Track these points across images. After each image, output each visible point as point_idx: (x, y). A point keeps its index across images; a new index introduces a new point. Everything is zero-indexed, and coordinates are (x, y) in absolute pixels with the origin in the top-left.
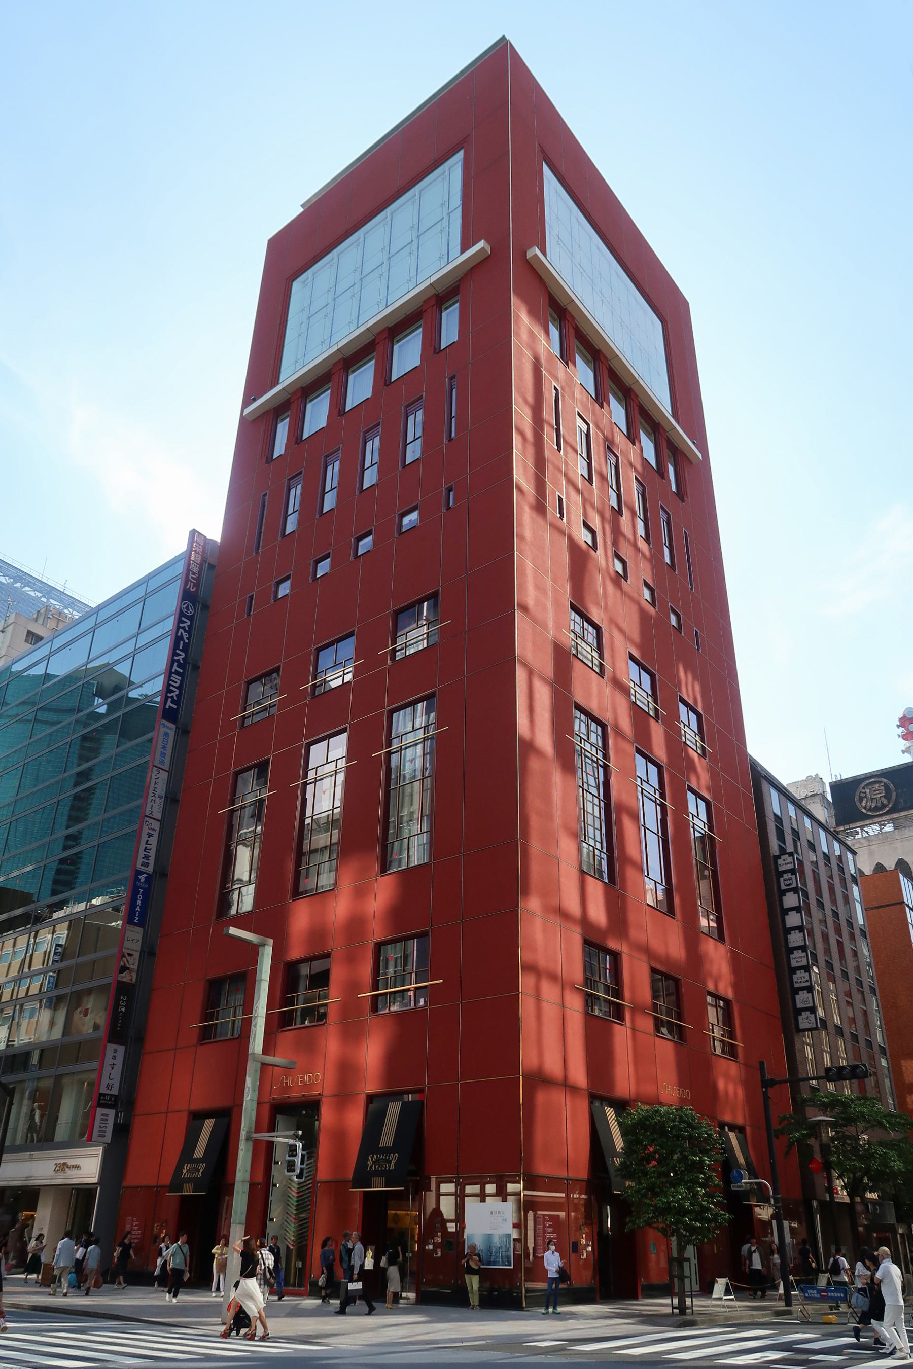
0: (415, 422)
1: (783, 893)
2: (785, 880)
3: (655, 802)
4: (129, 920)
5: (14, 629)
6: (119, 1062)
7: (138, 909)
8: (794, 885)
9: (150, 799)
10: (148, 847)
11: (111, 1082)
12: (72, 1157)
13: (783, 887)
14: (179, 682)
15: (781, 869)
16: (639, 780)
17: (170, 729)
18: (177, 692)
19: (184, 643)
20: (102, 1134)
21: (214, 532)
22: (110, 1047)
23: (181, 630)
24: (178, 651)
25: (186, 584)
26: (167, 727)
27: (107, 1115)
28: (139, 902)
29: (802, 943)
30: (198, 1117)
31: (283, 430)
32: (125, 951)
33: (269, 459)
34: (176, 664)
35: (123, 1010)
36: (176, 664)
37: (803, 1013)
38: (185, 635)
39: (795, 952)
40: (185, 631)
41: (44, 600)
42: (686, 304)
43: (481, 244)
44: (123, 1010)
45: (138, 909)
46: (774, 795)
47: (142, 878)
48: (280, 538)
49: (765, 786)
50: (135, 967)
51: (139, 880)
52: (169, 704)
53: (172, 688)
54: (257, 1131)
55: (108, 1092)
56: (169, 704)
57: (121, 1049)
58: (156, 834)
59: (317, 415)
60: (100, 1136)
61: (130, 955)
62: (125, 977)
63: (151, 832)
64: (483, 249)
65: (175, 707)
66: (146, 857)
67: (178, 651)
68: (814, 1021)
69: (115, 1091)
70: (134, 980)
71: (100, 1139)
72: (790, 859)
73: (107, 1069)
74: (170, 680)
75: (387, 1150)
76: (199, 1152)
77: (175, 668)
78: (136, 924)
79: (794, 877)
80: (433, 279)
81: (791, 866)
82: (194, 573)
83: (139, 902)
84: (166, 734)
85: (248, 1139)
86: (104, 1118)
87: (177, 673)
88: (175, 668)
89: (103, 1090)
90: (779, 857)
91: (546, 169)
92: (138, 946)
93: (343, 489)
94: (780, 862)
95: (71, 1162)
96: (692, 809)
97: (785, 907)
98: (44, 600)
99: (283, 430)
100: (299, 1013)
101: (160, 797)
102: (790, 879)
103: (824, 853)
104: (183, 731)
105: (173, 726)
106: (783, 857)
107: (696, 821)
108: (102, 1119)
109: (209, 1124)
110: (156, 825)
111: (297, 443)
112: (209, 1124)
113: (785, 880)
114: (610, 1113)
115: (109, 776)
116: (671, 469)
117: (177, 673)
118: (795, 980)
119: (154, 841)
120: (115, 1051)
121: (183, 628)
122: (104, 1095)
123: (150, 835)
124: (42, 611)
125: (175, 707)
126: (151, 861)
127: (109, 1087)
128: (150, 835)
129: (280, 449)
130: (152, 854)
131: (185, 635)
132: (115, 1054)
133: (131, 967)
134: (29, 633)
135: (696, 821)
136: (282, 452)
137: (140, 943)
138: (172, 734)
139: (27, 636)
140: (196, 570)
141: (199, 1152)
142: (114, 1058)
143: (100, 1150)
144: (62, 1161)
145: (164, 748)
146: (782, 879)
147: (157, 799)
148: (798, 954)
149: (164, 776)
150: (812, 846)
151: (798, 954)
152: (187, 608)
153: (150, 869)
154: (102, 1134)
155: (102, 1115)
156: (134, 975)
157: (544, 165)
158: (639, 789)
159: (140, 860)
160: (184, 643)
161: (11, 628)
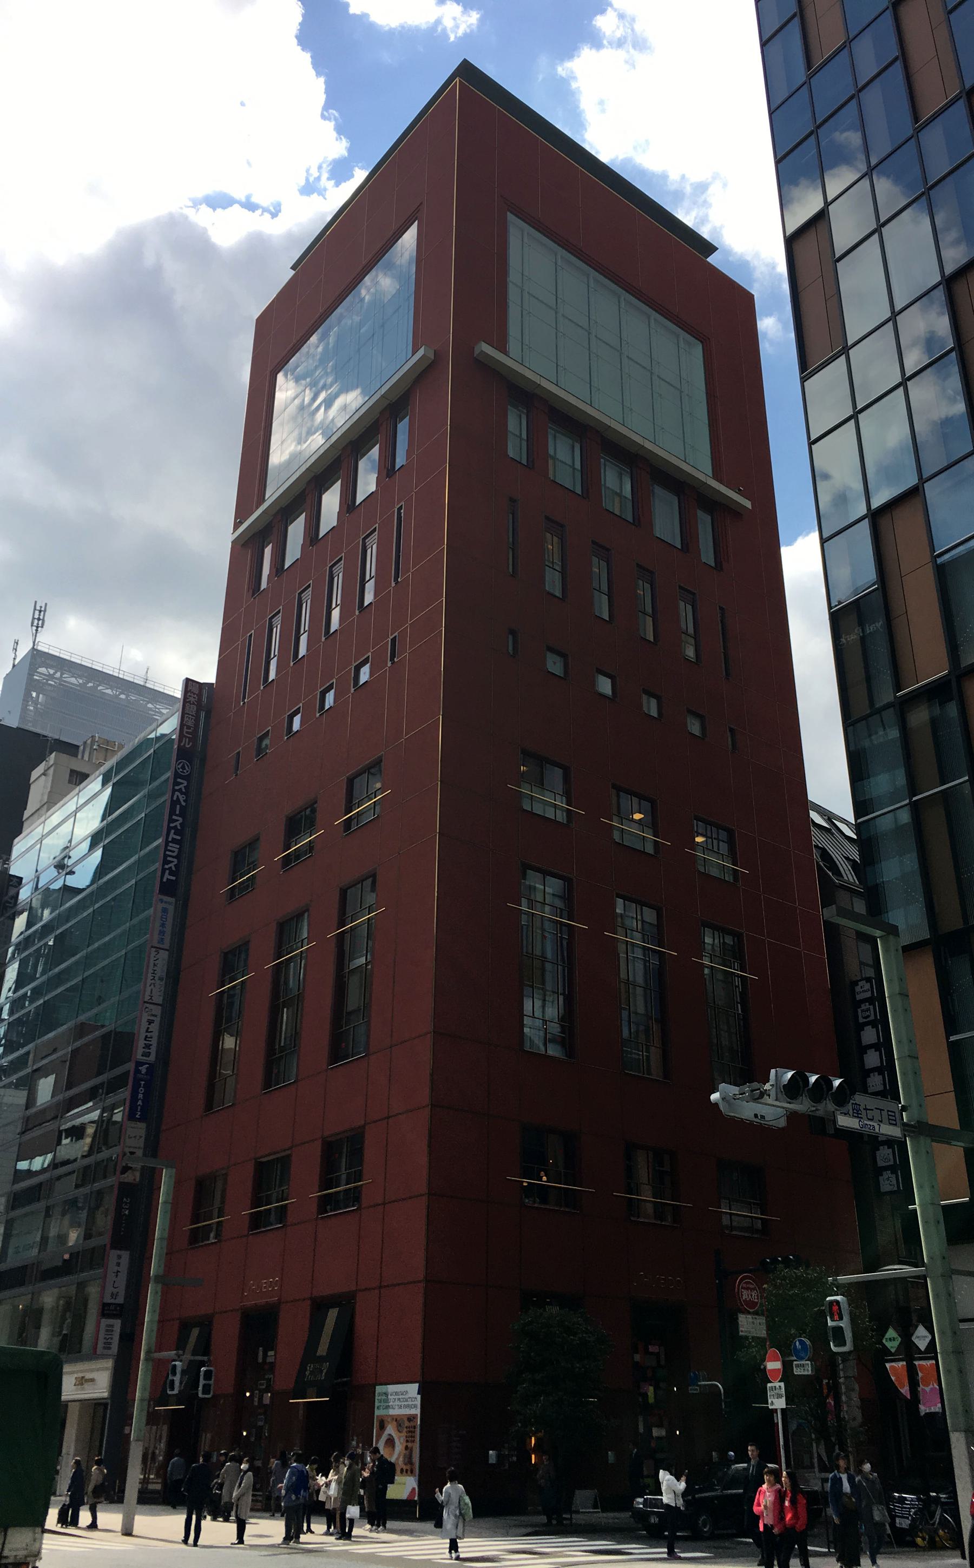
1: (861, 1027)
2: (862, 1011)
4: (131, 1116)
5: (55, 771)
6: (124, 1268)
7: (140, 1103)
8: (872, 1017)
9: (149, 982)
11: (115, 1291)
12: (92, 1371)
13: (861, 1020)
14: (176, 850)
17: (170, 903)
19: (181, 806)
20: (107, 1346)
22: (114, 1254)
24: (174, 817)
27: (112, 1326)
28: (141, 1096)
30: (319, 1306)
32: (127, 1150)
34: (173, 831)
35: (127, 1212)
36: (173, 831)
37: (884, 1173)
38: (182, 798)
40: (182, 793)
41: (123, 696)
44: (127, 1212)
45: (140, 1103)
47: (143, 1069)
48: (357, 612)
51: (140, 1072)
53: (169, 859)
54: (159, 1348)
55: (113, 1301)
56: (167, 876)
57: (125, 1255)
58: (157, 1020)
60: (104, 1348)
61: (132, 1153)
62: (129, 1177)
63: (152, 1018)
65: (174, 878)
67: (174, 817)
68: (895, 1182)
69: (120, 1300)
70: (138, 1180)
71: (106, 1352)
73: (111, 1277)
75: (321, 1359)
76: (322, 1350)
77: (172, 835)
78: (140, 1120)
79: (871, 1007)
81: (869, 994)
82: (189, 727)
83: (141, 1096)
85: (146, 1359)
86: (110, 1329)
87: (174, 841)
88: (172, 835)
89: (108, 1300)
92: (141, 1143)
95: (88, 1376)
97: (864, 1043)
98: (123, 696)
100: (273, 1213)
101: (161, 979)
102: (868, 1010)
104: (184, 906)
105: (172, 900)
108: (107, 1331)
109: (333, 1314)
110: (157, 1010)
111: (388, 476)
112: (333, 1314)
113: (862, 1011)
115: (80, 978)
117: (174, 841)
120: (119, 1257)
121: (180, 790)
122: (109, 1304)
123: (150, 1022)
124: (89, 742)
125: (174, 878)
126: (153, 1050)
127: (113, 1295)
128: (150, 1022)
131: (182, 798)
132: (119, 1261)
134: (72, 771)
138: (171, 909)
139: (70, 776)
141: (322, 1350)
142: (118, 1264)
143: (109, 1363)
144: (80, 1375)
146: (859, 1010)
147: (158, 982)
149: (164, 955)
152: (183, 768)
153: (152, 1058)
154: (107, 1346)
155: (107, 1326)
156: (138, 1174)
160: (181, 806)
161: (52, 770)
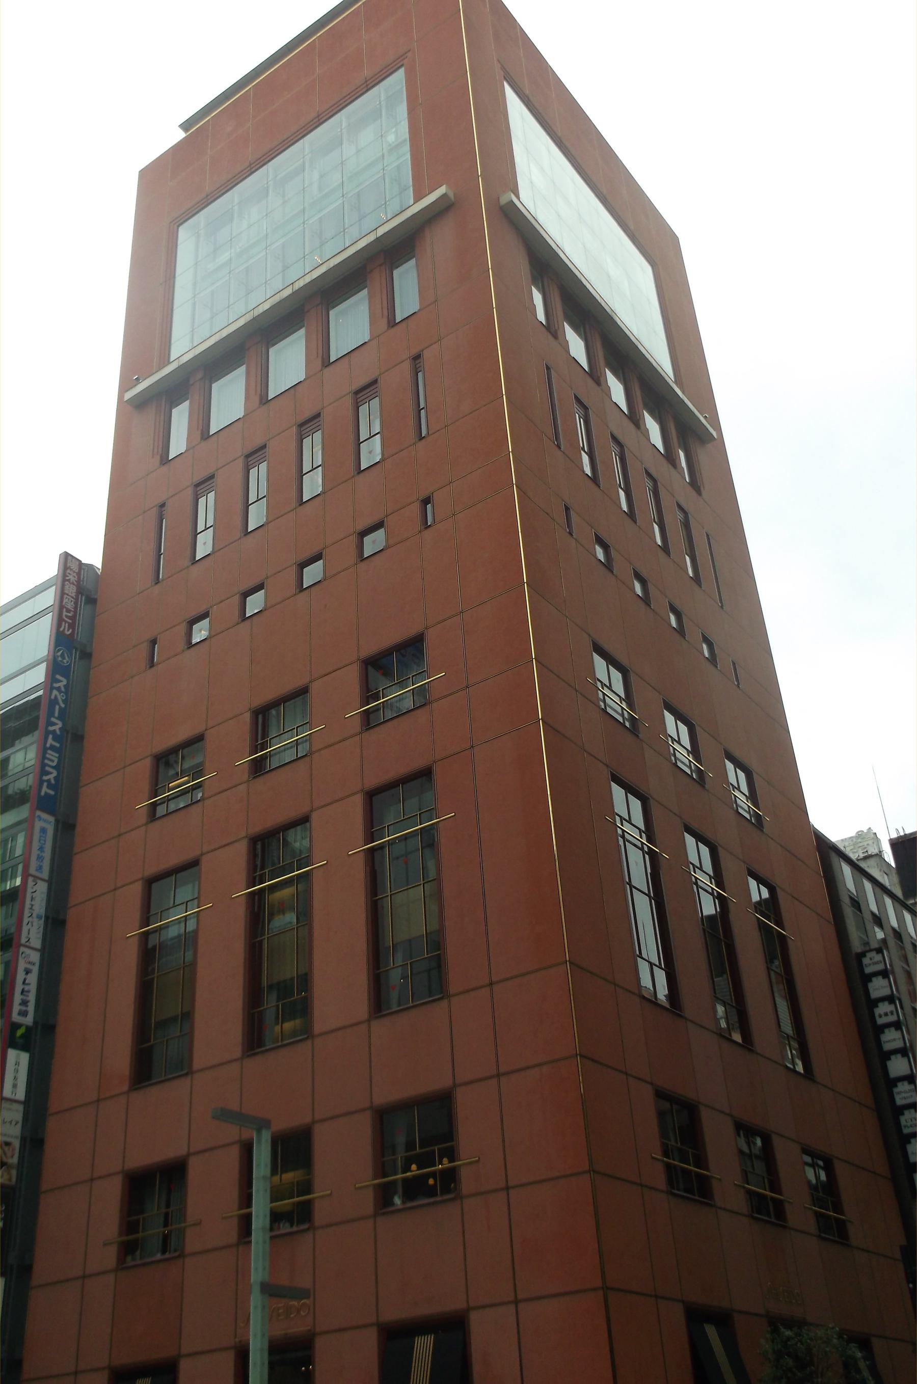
0: (371, 418)
3: (642, 849)
10: (26, 988)
14: (56, 760)
15: (868, 970)
16: (618, 818)
18: (55, 773)
19: (60, 707)
21: (92, 554)
23: (55, 692)
25: (59, 625)
26: (45, 821)
29: (908, 1072)
31: (181, 417)
33: (165, 460)
36: (51, 736)
39: (900, 1084)
40: (60, 692)
42: (674, 241)
43: (442, 190)
46: (847, 870)
49: (834, 858)
50: (15, 1160)
52: (45, 789)
53: (47, 768)
56: (45, 789)
58: (35, 970)
59: (229, 400)
63: (29, 966)
64: (444, 196)
66: (24, 1003)
67: (53, 719)
70: (14, 1179)
72: (878, 957)
74: (44, 758)
77: (50, 741)
80: (381, 232)
82: (68, 611)
84: (43, 831)
88: (50, 741)
90: (863, 954)
91: (510, 94)
93: (272, 496)
94: (866, 961)
96: (620, 806)
99: (181, 417)
101: (39, 917)
103: (873, 914)
105: (51, 819)
106: (869, 955)
107: (627, 827)
110: (35, 957)
114: (711, 1331)
116: (682, 455)
117: (52, 748)
118: (903, 1122)
119: (33, 979)
121: (58, 689)
123: (28, 972)
126: (31, 1008)
128: (28, 972)
129: (178, 444)
130: (32, 998)
133: (10, 1161)
135: (627, 827)
136: (183, 449)
137: (20, 1125)
140: (70, 606)
145: (41, 849)
148: (903, 1087)
150: (878, 921)
151: (903, 1087)
152: (62, 656)
156: (14, 1173)
157: (505, 83)
158: (619, 831)
159: (16, 1008)
160: (60, 707)
